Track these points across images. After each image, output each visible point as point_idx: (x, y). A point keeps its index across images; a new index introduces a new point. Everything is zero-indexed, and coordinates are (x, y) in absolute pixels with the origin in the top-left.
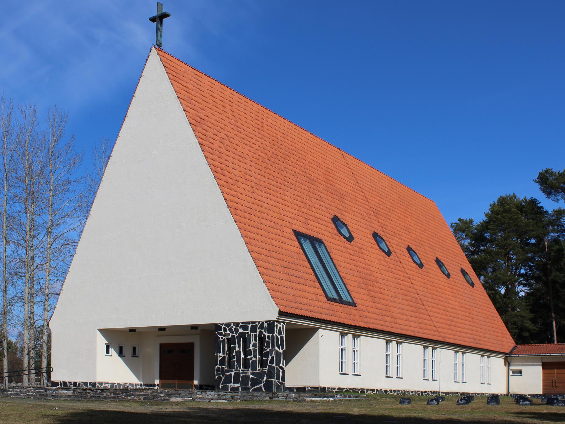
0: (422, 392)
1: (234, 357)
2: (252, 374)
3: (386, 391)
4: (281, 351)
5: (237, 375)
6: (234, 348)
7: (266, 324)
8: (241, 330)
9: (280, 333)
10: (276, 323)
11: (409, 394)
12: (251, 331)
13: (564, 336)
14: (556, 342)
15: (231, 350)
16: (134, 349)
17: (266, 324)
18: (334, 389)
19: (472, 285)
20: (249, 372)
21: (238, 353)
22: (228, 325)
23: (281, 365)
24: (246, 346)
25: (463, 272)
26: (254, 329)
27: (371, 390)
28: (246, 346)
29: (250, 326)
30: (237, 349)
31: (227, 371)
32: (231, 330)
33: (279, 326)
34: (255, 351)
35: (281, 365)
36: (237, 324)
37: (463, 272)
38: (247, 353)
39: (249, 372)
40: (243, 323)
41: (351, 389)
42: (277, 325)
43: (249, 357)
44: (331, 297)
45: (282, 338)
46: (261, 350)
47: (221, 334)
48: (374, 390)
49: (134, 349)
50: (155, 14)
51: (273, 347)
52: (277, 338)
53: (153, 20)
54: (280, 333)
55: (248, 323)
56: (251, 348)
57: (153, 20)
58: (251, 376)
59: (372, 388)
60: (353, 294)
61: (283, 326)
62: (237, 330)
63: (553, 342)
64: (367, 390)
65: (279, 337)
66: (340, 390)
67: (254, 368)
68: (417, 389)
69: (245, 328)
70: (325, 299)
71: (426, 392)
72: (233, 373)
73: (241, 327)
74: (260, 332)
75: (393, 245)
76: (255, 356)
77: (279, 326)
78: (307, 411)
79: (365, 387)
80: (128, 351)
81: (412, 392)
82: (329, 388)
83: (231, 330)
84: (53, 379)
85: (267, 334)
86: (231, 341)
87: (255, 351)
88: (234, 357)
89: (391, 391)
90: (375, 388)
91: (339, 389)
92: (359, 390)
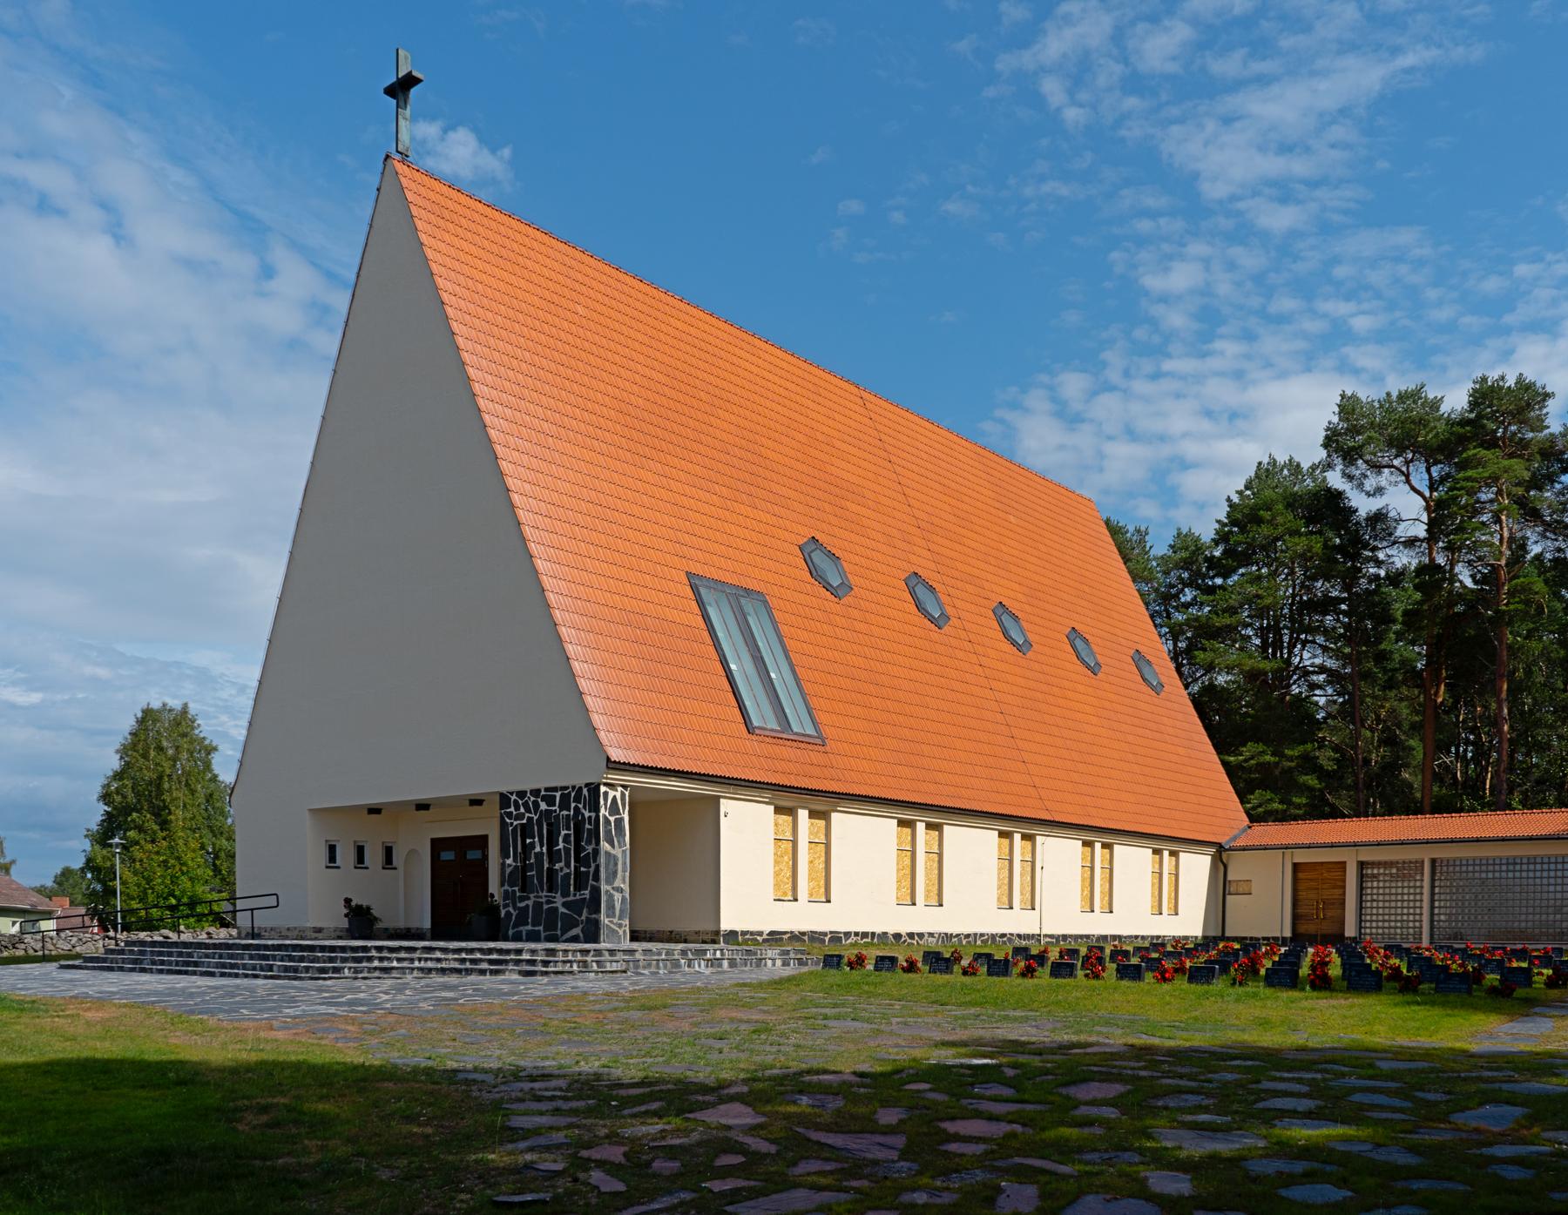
0: (993, 936)
1: (531, 867)
2: (564, 905)
3: (897, 936)
4: (617, 852)
5: (538, 905)
6: (532, 845)
7: (585, 791)
8: (543, 806)
9: (614, 809)
10: (603, 789)
13: (1563, 803)
15: (527, 849)
16: (389, 851)
17: (585, 791)
18: (760, 933)
19: (1157, 689)
22: (521, 794)
25: (1139, 659)
26: (565, 805)
27: (856, 934)
28: (552, 842)
29: (558, 795)
30: (538, 849)
31: (522, 899)
32: (526, 805)
33: (611, 794)
34: (567, 851)
36: (536, 793)
37: (1139, 659)
38: (553, 856)
39: (559, 901)
40: (547, 790)
41: (803, 934)
42: (606, 794)
43: (557, 866)
45: (619, 822)
46: (578, 849)
47: (510, 815)
48: (865, 935)
51: (598, 843)
52: (607, 822)
53: (391, 91)
54: (614, 809)
55: (555, 789)
56: (561, 846)
57: (391, 91)
58: (562, 910)
59: (860, 930)
60: (822, 717)
61: (623, 795)
62: (536, 805)
64: (847, 934)
65: (612, 819)
66: (775, 937)
68: (980, 930)
69: (550, 801)
71: (1003, 935)
72: (530, 903)
74: (576, 808)
75: (959, 603)
76: (568, 865)
77: (611, 794)
78: (254, 1057)
79: (842, 927)
81: (968, 936)
82: (744, 933)
83: (526, 805)
85: (587, 814)
86: (526, 831)
87: (567, 851)
88: (531, 867)
89: (911, 935)
90: (870, 930)
91: (772, 933)
92: (825, 934)
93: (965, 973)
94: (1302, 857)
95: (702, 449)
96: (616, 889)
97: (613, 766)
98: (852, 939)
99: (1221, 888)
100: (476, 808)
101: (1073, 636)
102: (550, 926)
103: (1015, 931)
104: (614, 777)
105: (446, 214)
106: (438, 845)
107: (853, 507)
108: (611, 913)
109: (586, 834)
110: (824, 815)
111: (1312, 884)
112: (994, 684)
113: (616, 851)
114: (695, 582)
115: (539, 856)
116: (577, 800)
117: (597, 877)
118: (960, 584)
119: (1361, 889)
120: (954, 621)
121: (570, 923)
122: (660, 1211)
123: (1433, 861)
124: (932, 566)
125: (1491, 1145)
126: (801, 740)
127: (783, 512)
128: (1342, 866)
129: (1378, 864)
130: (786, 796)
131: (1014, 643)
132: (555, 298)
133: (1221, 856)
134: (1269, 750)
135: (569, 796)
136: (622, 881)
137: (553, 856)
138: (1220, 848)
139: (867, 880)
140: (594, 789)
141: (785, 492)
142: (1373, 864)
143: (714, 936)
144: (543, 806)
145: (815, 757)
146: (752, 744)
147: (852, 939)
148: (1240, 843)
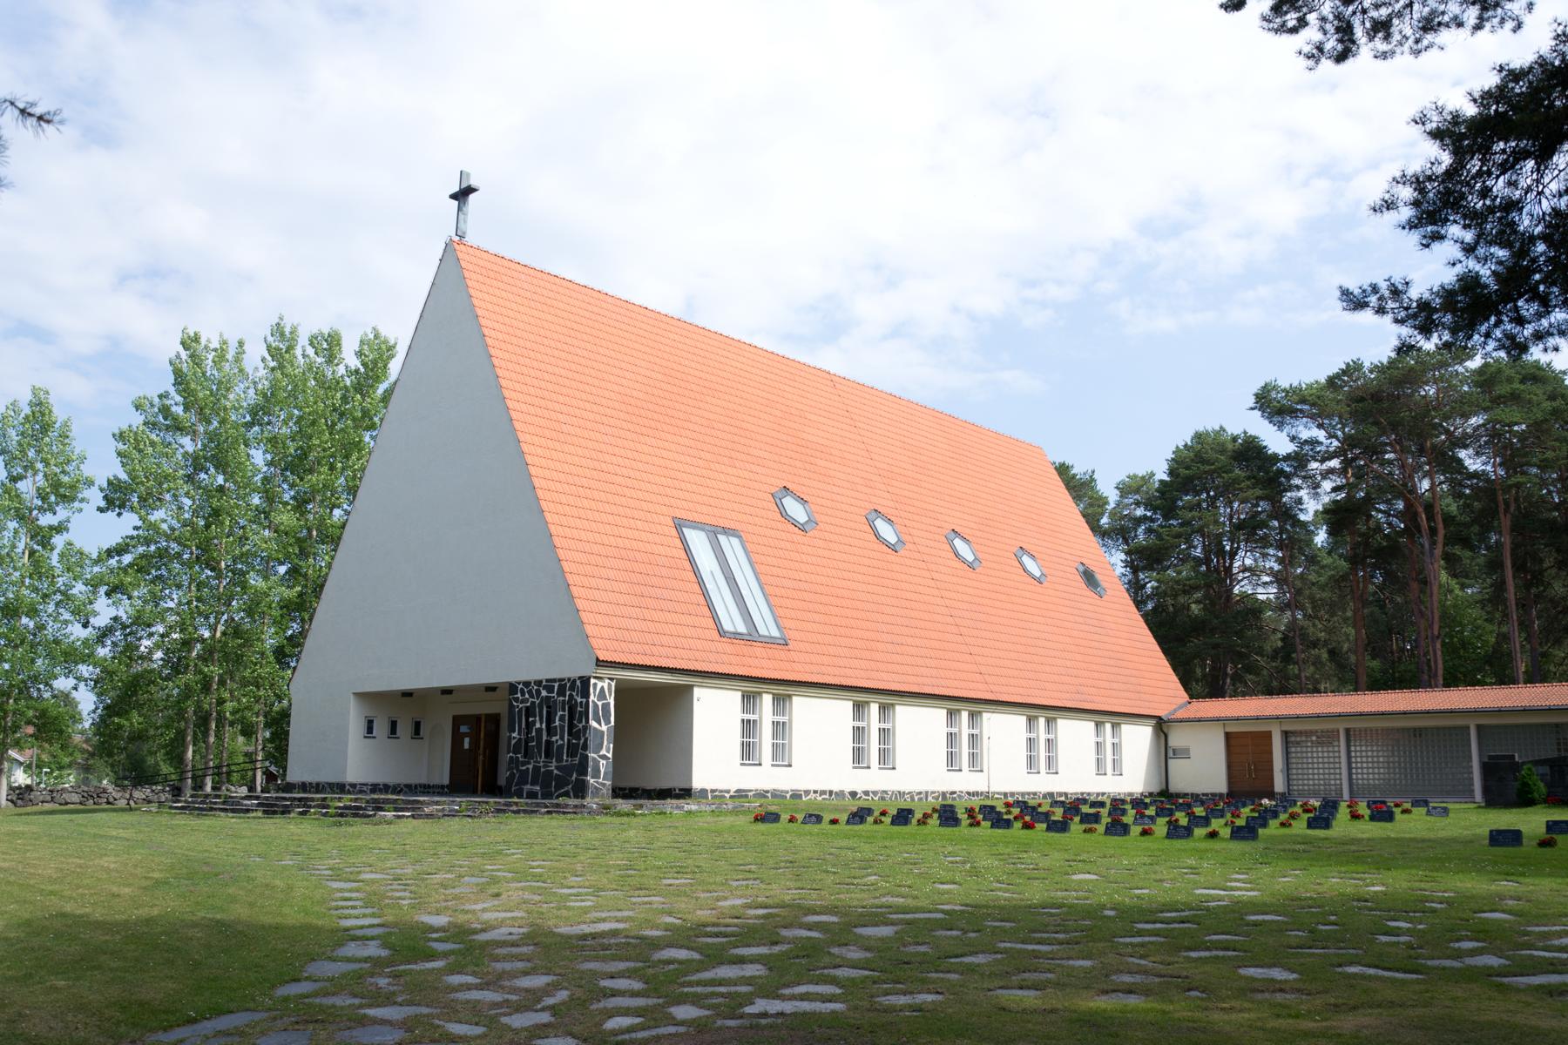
4: (604, 728)
5: (536, 769)
8: (544, 693)
10: (593, 681)
11: (912, 799)
12: (559, 694)
14: (603, 692)
15: (529, 726)
16: (417, 726)
20: (553, 765)
21: (539, 731)
22: (527, 684)
23: (603, 752)
24: (550, 721)
26: (561, 692)
28: (550, 721)
31: (524, 764)
33: (600, 684)
34: (562, 728)
35: (603, 752)
36: (539, 683)
38: (551, 731)
39: (553, 765)
44: (731, 629)
46: (571, 726)
47: (517, 700)
48: (823, 792)
49: (417, 726)
50: (456, 189)
52: (596, 706)
53: (454, 197)
54: (602, 695)
55: (554, 681)
57: (454, 197)
59: (819, 787)
62: (538, 692)
63: (625, 693)
64: (807, 792)
67: (560, 759)
68: (930, 788)
69: (550, 689)
70: (717, 636)
73: (545, 687)
76: (562, 738)
79: (801, 786)
80: (404, 729)
82: (713, 791)
83: (530, 692)
84: (295, 774)
86: (529, 712)
87: (562, 728)
89: (866, 793)
93: (876, 822)
94: (1233, 728)
95: (691, 426)
96: (603, 756)
97: (600, 663)
98: (812, 796)
99: (1165, 751)
100: (1080, 583)
101: (1020, 553)
102: (545, 784)
103: (965, 789)
104: (603, 672)
105: (492, 274)
106: (457, 721)
107: (822, 463)
108: (596, 774)
109: (578, 715)
110: (781, 701)
111: (1246, 749)
112: (945, 594)
113: (602, 728)
114: (679, 525)
115: (539, 731)
116: (572, 688)
117: (585, 747)
118: (916, 518)
119: (1287, 754)
120: (909, 546)
121: (561, 782)
122: (1306, 1034)
123: (1348, 731)
124: (891, 504)
125: (628, 970)
126: (769, 642)
127: (758, 469)
128: (1268, 735)
129: (1301, 733)
130: (751, 685)
131: (964, 561)
132: (575, 326)
133: (1161, 726)
134: (1203, 639)
135: (564, 685)
136: (607, 750)
137: (551, 731)
138: (1160, 718)
139: (820, 752)
140: (585, 681)
141: (761, 454)
142: (1294, 733)
143: (686, 793)
144: (544, 693)
145: (783, 654)
146: (724, 646)
147: (812, 796)
148: (1180, 715)
